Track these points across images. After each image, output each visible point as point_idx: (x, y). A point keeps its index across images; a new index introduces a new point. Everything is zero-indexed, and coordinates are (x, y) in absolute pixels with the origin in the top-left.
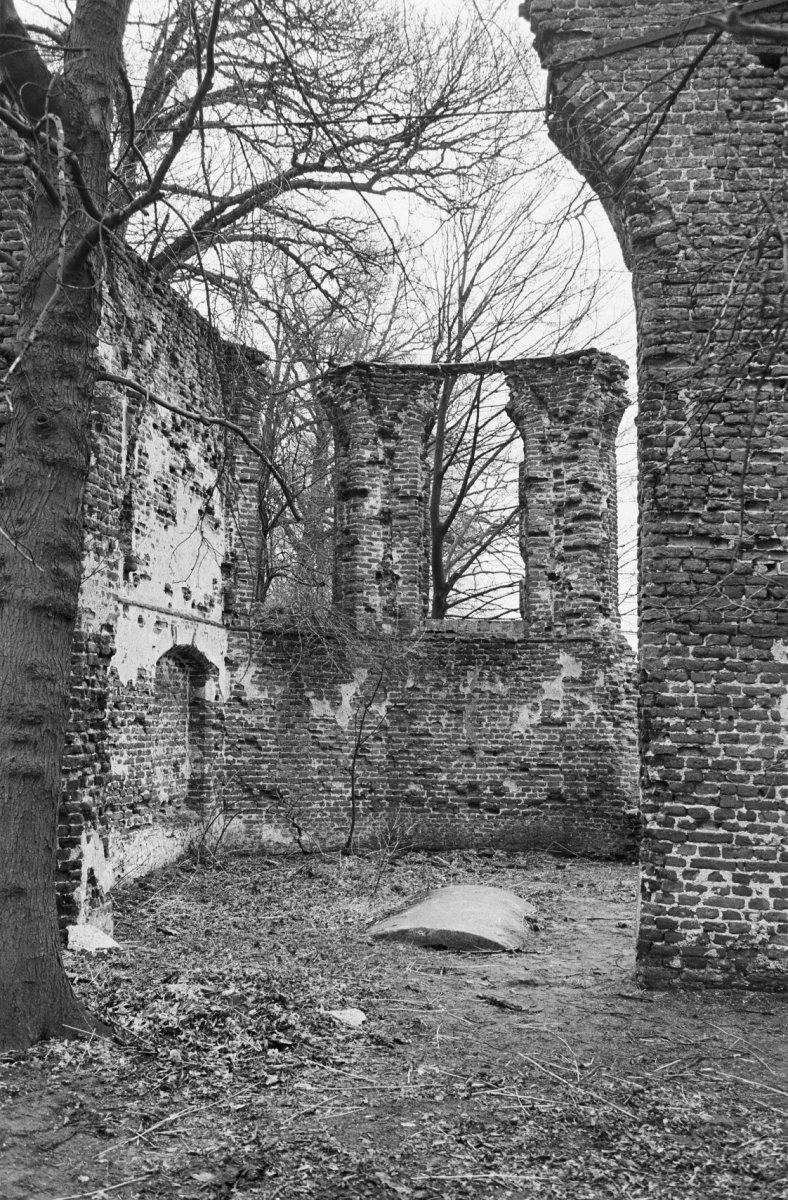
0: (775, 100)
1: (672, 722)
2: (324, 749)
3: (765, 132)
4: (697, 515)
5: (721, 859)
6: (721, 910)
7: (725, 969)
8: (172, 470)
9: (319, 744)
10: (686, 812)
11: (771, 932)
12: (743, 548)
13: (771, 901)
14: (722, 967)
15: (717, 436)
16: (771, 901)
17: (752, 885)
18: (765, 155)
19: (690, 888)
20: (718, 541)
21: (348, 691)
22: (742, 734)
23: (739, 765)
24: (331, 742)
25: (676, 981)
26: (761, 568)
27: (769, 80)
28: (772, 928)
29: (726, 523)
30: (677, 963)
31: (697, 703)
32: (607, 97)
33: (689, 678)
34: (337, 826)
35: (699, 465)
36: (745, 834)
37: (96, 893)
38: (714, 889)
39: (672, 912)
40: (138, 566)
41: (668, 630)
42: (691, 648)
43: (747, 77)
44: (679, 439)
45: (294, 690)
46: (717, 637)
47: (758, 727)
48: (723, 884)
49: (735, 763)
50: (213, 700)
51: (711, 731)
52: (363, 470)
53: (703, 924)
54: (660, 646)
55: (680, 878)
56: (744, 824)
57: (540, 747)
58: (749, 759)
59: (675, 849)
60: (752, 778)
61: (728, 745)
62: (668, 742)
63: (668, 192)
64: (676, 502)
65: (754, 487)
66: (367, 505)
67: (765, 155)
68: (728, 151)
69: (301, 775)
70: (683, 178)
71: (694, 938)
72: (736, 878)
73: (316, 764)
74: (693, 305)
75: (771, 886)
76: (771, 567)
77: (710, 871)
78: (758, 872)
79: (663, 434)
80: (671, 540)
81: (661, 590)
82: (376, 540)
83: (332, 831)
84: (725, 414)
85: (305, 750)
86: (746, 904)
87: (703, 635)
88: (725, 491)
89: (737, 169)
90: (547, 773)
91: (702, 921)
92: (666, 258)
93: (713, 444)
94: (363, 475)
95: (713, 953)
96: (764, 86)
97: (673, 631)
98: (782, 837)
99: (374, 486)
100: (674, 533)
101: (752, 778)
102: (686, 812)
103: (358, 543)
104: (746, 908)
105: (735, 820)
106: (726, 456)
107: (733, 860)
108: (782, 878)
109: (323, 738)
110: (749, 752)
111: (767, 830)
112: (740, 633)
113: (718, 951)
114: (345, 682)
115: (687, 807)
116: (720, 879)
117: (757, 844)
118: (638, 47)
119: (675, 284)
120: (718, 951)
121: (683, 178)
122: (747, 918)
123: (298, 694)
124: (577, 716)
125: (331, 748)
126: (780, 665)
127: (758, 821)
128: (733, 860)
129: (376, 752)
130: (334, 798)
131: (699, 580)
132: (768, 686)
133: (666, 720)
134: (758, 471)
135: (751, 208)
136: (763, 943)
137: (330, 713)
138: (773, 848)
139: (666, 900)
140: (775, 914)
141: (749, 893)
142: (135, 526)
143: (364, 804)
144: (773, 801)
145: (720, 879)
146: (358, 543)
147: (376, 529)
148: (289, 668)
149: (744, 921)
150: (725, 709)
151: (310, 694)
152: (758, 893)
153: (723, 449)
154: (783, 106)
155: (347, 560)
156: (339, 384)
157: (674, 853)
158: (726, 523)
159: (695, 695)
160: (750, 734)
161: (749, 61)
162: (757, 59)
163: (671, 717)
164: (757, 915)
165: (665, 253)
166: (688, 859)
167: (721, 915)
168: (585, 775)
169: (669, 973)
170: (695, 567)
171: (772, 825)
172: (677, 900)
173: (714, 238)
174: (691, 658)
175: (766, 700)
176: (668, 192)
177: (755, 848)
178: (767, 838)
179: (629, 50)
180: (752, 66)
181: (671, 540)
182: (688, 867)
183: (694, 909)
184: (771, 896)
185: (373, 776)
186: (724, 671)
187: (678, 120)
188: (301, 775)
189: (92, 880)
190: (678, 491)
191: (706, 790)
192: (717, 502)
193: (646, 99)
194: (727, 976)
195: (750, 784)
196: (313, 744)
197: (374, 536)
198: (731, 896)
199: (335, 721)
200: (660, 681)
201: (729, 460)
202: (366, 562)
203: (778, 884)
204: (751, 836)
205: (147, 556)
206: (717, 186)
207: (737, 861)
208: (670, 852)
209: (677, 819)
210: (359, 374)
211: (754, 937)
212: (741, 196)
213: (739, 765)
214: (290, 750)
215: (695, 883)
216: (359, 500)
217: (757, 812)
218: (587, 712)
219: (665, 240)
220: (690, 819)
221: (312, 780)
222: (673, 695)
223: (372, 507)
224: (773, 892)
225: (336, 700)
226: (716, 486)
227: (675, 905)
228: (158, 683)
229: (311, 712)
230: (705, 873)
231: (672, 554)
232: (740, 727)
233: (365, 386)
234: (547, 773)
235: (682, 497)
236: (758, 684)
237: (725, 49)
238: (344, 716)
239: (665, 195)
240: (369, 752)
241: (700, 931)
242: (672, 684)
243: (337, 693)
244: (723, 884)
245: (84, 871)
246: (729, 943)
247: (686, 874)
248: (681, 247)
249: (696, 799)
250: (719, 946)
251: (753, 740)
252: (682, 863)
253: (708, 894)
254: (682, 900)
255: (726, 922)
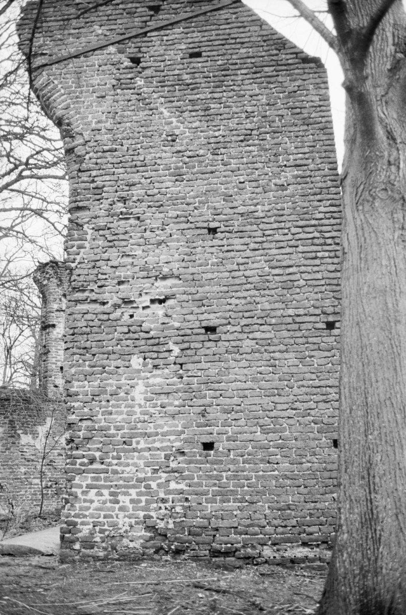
0: (137, 79)
1: (76, 405)
2: (28, 461)
3: (132, 94)
4: (92, 290)
5: (102, 483)
6: (102, 513)
7: (105, 549)
9: (25, 459)
10: (84, 456)
11: (131, 526)
12: (116, 306)
13: (131, 506)
14: (103, 548)
15: (103, 248)
16: (131, 506)
17: (120, 498)
18: (131, 105)
19: (85, 501)
20: (104, 304)
21: (42, 430)
22: (114, 410)
23: (112, 427)
24: (32, 457)
25: (77, 557)
26: (126, 317)
27: (134, 70)
28: (131, 522)
29: (107, 293)
30: (77, 546)
31: (89, 394)
32: (54, 83)
33: (86, 379)
34: (35, 503)
35: (93, 264)
36: (115, 467)
38: (98, 501)
39: (76, 516)
41: (74, 354)
42: (87, 363)
43: (124, 69)
45: (10, 429)
46: (101, 356)
47: (123, 406)
48: (103, 498)
49: (110, 426)
52: (52, 314)
53: (93, 522)
54: (70, 363)
55: (80, 495)
56: (115, 462)
58: (118, 424)
59: (77, 478)
60: (120, 435)
61: (106, 416)
62: (74, 417)
63: (81, 126)
64: (80, 284)
65: (122, 273)
66: (55, 332)
67: (131, 105)
68: (113, 105)
69: (14, 475)
70: (90, 119)
71: (88, 531)
72: (111, 494)
73: (23, 470)
74: (93, 181)
75: (130, 497)
76: (132, 316)
77: (97, 490)
78: (123, 490)
79: (75, 249)
80: (78, 304)
82: (59, 350)
83: (32, 506)
85: (17, 462)
86: (117, 509)
87: (94, 355)
88: (107, 276)
89: (117, 113)
91: (92, 520)
92: (80, 159)
93: (100, 252)
94: (53, 317)
95: (98, 539)
96: (132, 72)
97: (77, 354)
98: (137, 468)
99: (59, 322)
100: (79, 300)
101: (120, 435)
102: (84, 456)
103: (50, 352)
104: (117, 512)
105: (110, 460)
106: (107, 258)
107: (110, 483)
108: (137, 493)
109: (27, 456)
110: (118, 420)
111: (128, 465)
112: (114, 353)
113: (101, 538)
114: (41, 425)
115: (84, 453)
116: (102, 495)
117: (123, 473)
118: (69, 58)
119: (84, 171)
120: (101, 538)
121: (90, 119)
122: (117, 517)
123: (13, 431)
125: (33, 461)
126: (135, 370)
127: (122, 460)
128: (110, 483)
129: (59, 462)
130: (34, 488)
131: (92, 325)
132: (129, 382)
133: (73, 404)
134: (124, 265)
135: (123, 131)
136: (126, 532)
137: (32, 442)
138: (132, 475)
139: (72, 509)
140: (133, 514)
141: (117, 502)
143: (52, 491)
144: (131, 447)
145: (102, 495)
146: (50, 352)
147: (60, 344)
148: (8, 417)
149: (115, 519)
150: (105, 396)
151: (20, 432)
152: (123, 502)
153: (106, 254)
154: (141, 81)
155: (44, 361)
156: (43, 272)
157: (77, 481)
158: (107, 293)
159: (89, 389)
160: (119, 409)
161: (125, 61)
162: (129, 60)
163: (75, 402)
164: (123, 515)
165: (79, 156)
166: (84, 484)
167: (102, 516)
169: (73, 553)
170: (89, 319)
171: (130, 461)
172: (78, 509)
173: (105, 147)
175: (127, 389)
176: (81, 126)
177: (121, 475)
178: (128, 469)
179: (65, 60)
180: (126, 64)
181: (78, 304)
182: (84, 489)
183: (87, 513)
184: (131, 503)
185: (57, 475)
186: (105, 374)
187: (88, 91)
188: (14, 475)
190: (82, 278)
191: (94, 443)
192: (103, 282)
193: (73, 82)
194: (106, 553)
195: (119, 438)
196: (22, 458)
197: (59, 348)
198: (108, 505)
199: (35, 446)
200: (70, 382)
201: (109, 260)
202: (55, 362)
203: (134, 496)
204: (119, 469)
206: (107, 122)
207: (112, 484)
208: (74, 480)
209: (79, 461)
210: (53, 267)
211: (120, 529)
212: (118, 126)
213: (112, 427)
214: (8, 462)
215: (88, 498)
216: (51, 329)
217: (122, 454)
219: (80, 151)
220: (85, 460)
221: (20, 479)
222: (77, 390)
223: (58, 333)
224: (132, 501)
225: (35, 435)
226: (102, 274)
229: (21, 441)
230: (93, 491)
231: (77, 312)
232: (113, 406)
233: (56, 272)
235: (84, 281)
236: (123, 381)
237: (113, 57)
238: (39, 444)
239: (80, 128)
240: (55, 462)
241: (91, 526)
243: (36, 431)
244: (103, 498)
246: (107, 533)
247: (83, 492)
248: (87, 153)
249: (89, 448)
250: (102, 535)
251: (121, 413)
252: (80, 486)
253: (96, 505)
254: (81, 509)
255: (105, 520)
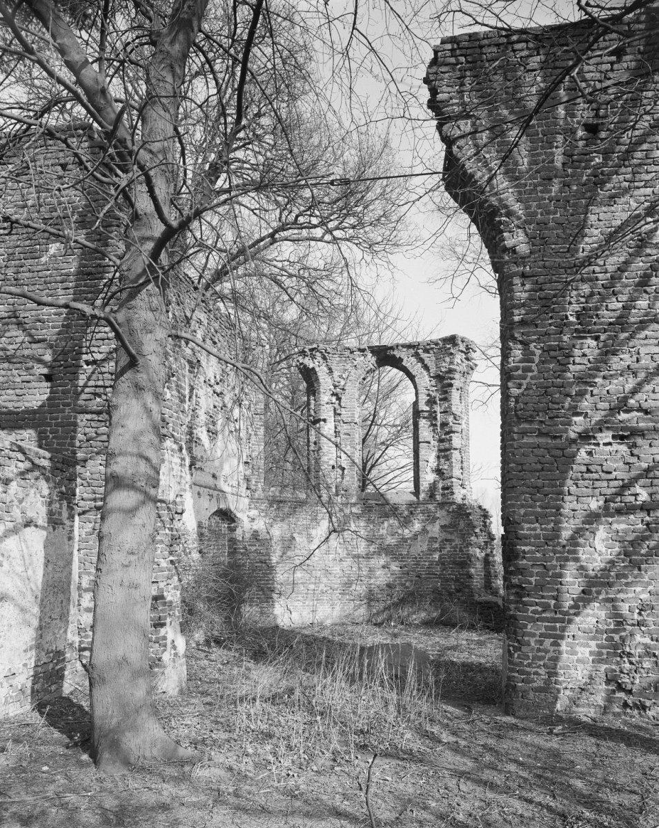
1: (526, 548)
8: (215, 407)
10: (537, 604)
37: (176, 655)
40: (197, 463)
44: (530, 374)
50: (241, 539)
51: (552, 554)
57: (427, 563)
59: (529, 627)
80: (525, 438)
81: (520, 467)
84: (560, 358)
90: (431, 578)
97: (527, 493)
102: (537, 604)
115: (537, 600)
124: (448, 546)
142: (195, 439)
168: (452, 579)
174: (539, 510)
189: (174, 647)
205: (202, 457)
206: (555, 213)
218: (454, 544)
220: (540, 609)
226: (553, 403)
227: (530, 661)
228: (210, 530)
232: (568, 552)
234: (431, 578)
242: (526, 526)
245: (169, 642)
252: (534, 635)
